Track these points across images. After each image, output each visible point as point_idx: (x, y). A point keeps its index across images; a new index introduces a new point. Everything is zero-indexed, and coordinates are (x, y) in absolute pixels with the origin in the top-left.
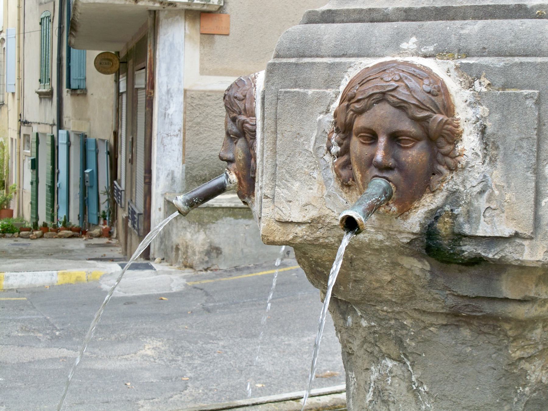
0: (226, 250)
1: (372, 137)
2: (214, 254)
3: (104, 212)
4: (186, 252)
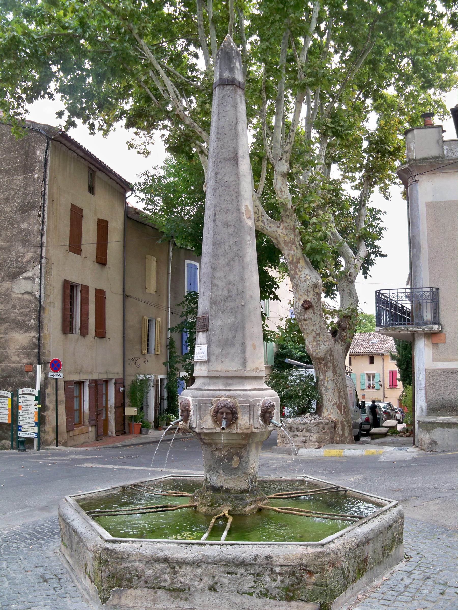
0: (439, 442)
1: (222, 413)
2: (434, 444)
4: (421, 443)
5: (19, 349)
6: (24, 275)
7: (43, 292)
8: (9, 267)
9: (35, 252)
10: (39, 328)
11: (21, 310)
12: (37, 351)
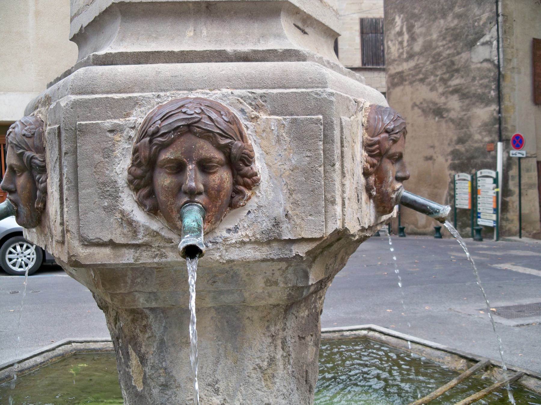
3: (488, 381)
5: (480, 127)
6: (482, 40)
7: (501, 56)
8: (467, 35)
9: (491, 11)
10: (499, 99)
11: (481, 82)
12: (499, 127)
